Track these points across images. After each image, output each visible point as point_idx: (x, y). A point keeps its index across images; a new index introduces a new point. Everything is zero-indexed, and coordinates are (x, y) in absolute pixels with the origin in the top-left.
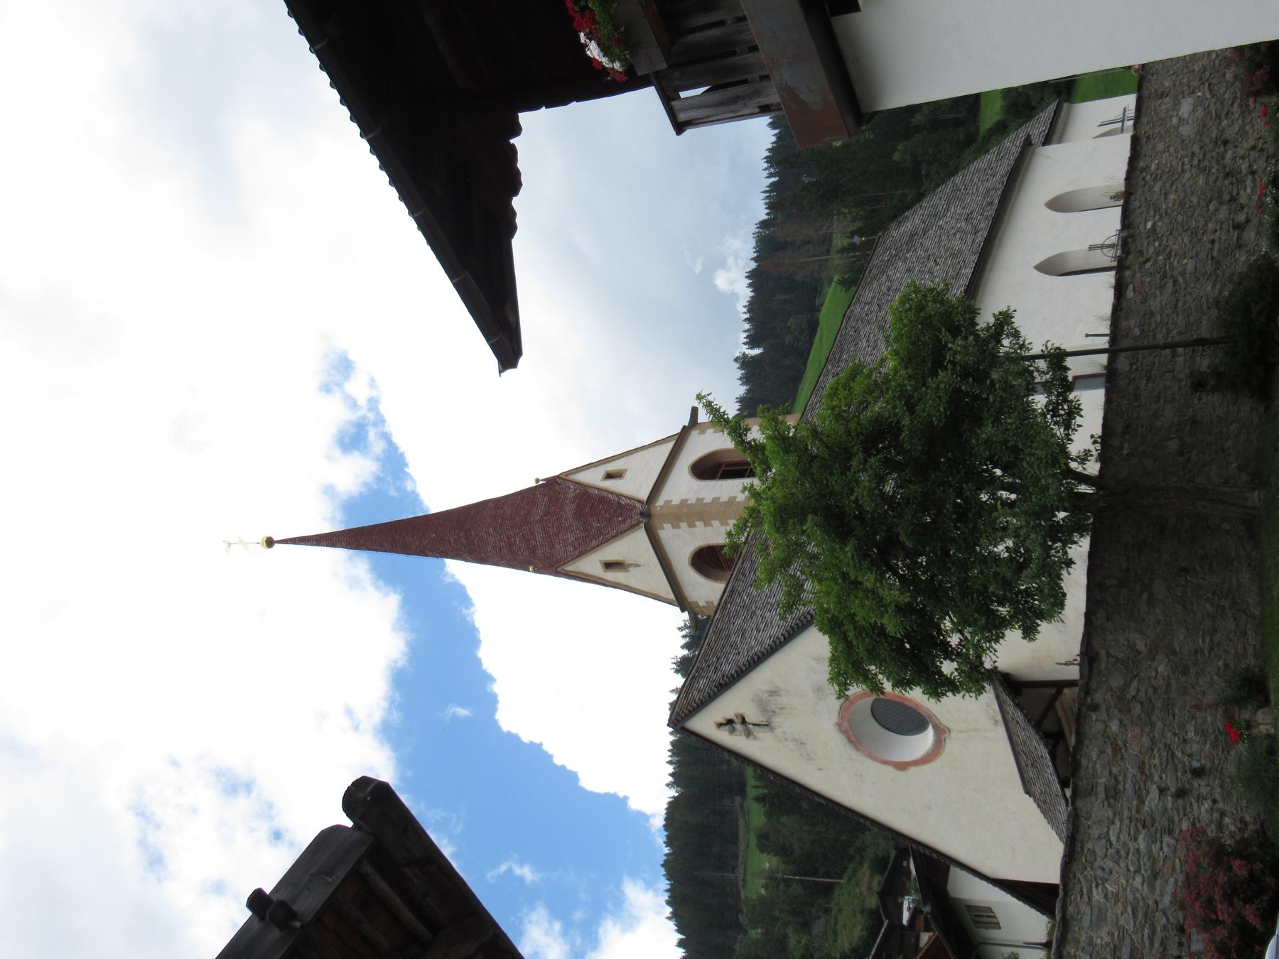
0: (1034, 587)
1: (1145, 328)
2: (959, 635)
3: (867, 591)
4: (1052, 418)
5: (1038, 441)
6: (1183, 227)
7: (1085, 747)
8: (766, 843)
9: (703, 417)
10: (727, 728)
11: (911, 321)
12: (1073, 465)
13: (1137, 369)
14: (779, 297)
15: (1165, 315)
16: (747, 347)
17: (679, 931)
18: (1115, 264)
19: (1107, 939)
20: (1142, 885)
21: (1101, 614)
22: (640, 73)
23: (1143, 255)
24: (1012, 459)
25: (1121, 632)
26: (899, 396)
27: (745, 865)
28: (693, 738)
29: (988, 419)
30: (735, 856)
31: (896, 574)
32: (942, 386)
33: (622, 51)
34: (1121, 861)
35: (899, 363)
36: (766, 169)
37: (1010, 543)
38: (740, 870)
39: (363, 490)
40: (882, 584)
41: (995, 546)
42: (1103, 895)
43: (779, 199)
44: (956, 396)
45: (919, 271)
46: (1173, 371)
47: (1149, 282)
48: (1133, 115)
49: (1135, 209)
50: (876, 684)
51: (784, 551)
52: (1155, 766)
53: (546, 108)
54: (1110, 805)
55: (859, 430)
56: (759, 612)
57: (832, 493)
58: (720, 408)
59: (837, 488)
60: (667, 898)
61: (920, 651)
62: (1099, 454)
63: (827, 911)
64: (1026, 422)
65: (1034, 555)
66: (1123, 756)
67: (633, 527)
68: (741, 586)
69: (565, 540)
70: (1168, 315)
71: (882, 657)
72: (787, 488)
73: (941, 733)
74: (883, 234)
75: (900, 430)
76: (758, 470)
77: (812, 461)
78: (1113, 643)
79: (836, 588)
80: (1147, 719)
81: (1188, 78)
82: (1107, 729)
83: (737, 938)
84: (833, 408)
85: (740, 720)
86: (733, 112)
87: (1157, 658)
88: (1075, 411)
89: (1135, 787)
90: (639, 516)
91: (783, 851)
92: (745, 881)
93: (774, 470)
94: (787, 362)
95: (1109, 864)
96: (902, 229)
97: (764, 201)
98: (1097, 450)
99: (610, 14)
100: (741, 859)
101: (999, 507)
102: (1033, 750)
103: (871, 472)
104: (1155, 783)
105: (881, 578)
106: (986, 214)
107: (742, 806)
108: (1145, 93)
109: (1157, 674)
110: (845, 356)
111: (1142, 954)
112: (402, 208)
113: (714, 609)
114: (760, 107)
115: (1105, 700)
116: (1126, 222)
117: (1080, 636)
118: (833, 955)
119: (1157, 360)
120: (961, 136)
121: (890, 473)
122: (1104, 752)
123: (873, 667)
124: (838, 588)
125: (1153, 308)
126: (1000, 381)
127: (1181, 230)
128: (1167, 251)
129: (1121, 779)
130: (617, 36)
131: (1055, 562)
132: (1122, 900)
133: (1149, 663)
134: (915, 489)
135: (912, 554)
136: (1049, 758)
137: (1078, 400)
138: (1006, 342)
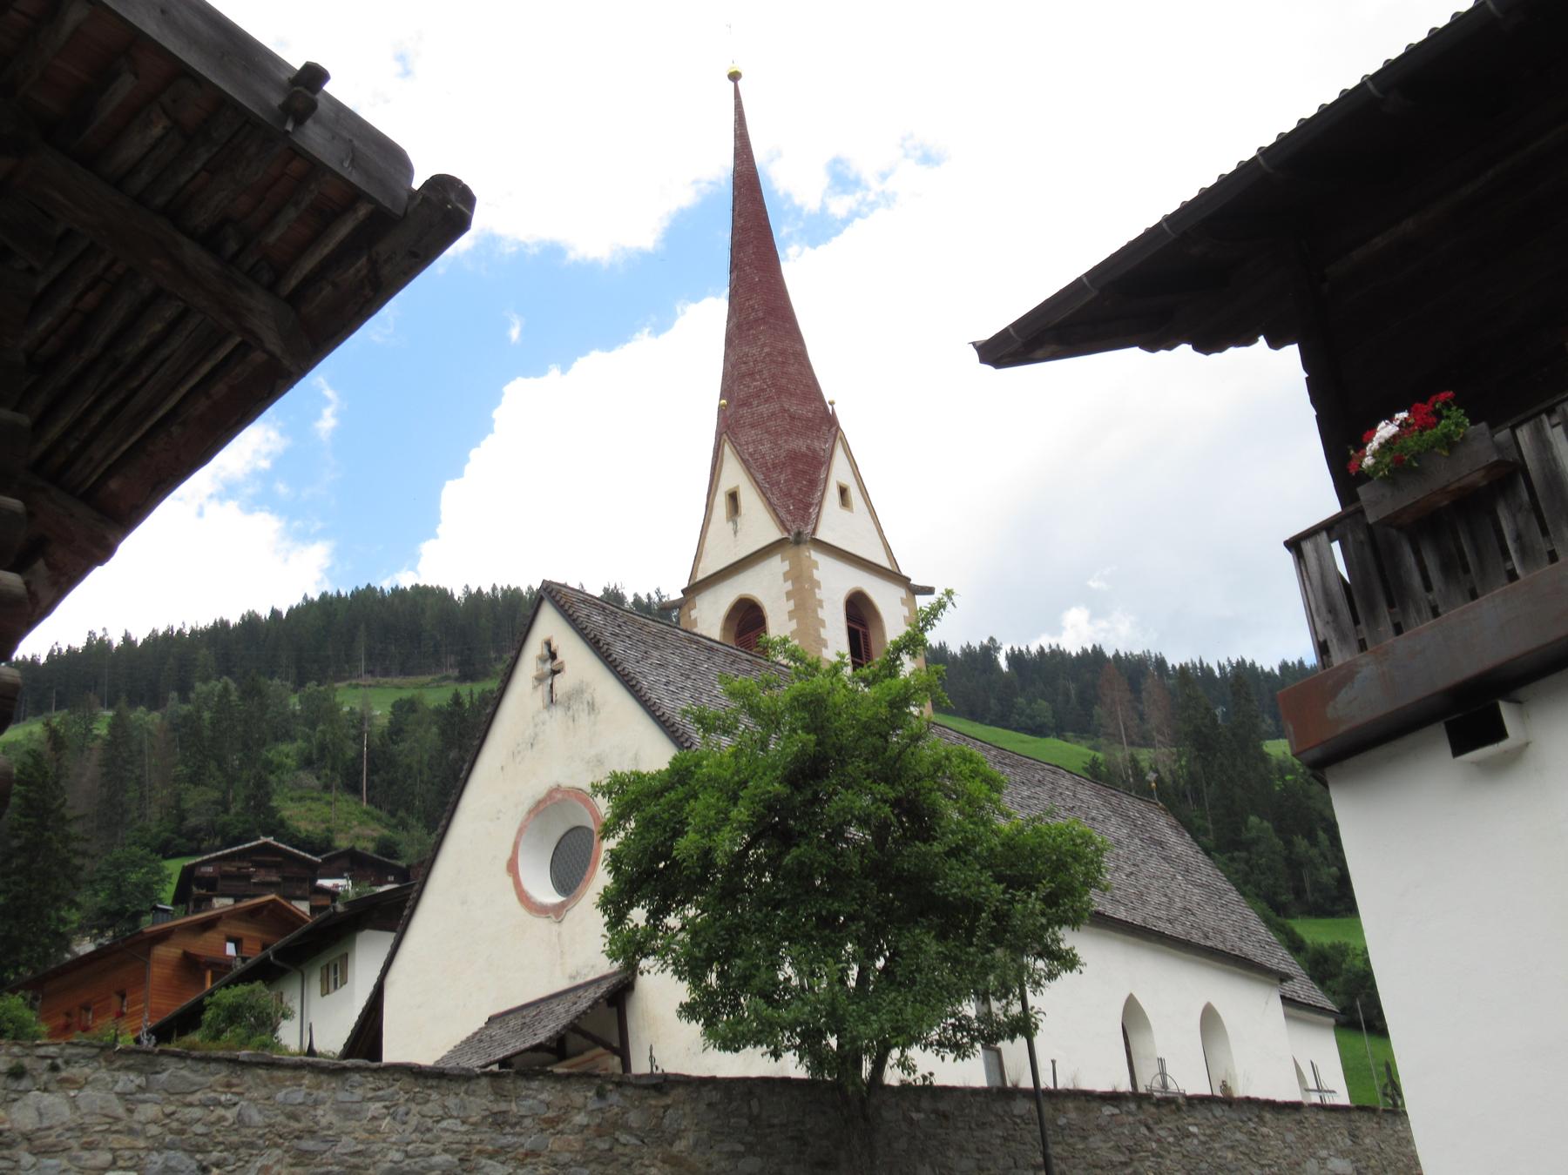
0: (744, 1013)
1: (1067, 1132)
2: (679, 926)
3: (727, 812)
4: (952, 1024)
5: (922, 1009)
6: (1192, 1170)
7: (552, 1085)
8: (404, 709)
9: (923, 602)
10: (546, 652)
11: (1060, 847)
12: (895, 1053)
13: (1015, 1123)
14: (1072, 687)
15: (1085, 1154)
16: (1009, 652)
17: (291, 611)
18: (1142, 1089)
19: (324, 1122)
20: (391, 1161)
21: (716, 1096)
22: (1361, 490)
23: (1156, 1123)
24: (898, 979)
25: (696, 1121)
26: (967, 838)
27: (375, 686)
28: (530, 613)
29: (946, 947)
30: (386, 673)
31: (749, 846)
32: (983, 889)
33: (1387, 466)
34: (418, 1135)
35: (1007, 836)
36: (1229, 661)
37: (795, 982)
38: (370, 680)
39: (781, 193)
40: (737, 830)
41: (790, 964)
42: (376, 1114)
43: (1193, 680)
44: (972, 907)
45: (1118, 855)
46: (1016, 1167)
47: (1123, 1133)
48: (1328, 1102)
49: (1211, 1111)
50: (612, 831)
51: (769, 708)
52: (536, 1169)
53: (1307, 379)
54: (485, 1118)
55: (922, 791)
56: (689, 683)
57: (843, 763)
58: (939, 619)
59: (850, 768)
60: (330, 593)
61: (656, 880)
62: (910, 1084)
63: (327, 788)
64: (945, 993)
65: (783, 1012)
66: (546, 1130)
67: (782, 524)
68: (719, 660)
69: (761, 442)
70: (1084, 1157)
71: (647, 835)
72: (847, 707)
73: (557, 912)
74: (1161, 808)
75: (925, 841)
76: (865, 671)
77: (881, 736)
78: (681, 1112)
79: (727, 775)
80: (592, 1158)
81: (1377, 1167)
82: (576, 1111)
83: (287, 680)
84: (947, 758)
85: (555, 668)
86: (1318, 609)
87: (666, 1166)
88: (960, 1051)
89: (509, 1147)
90: (796, 530)
91: (396, 731)
92: (357, 686)
93: (866, 690)
94: (993, 701)
95: (414, 1121)
96: (1168, 831)
97: (1189, 662)
98: (915, 1081)
99: (1433, 447)
100: (382, 680)
101: (841, 966)
102: (543, 1024)
103: (873, 808)
104: (515, 1170)
105: (742, 827)
106: (1194, 931)
107: (447, 678)
108: (1355, 1116)
109: (647, 1166)
110: (1008, 770)
111: (308, 1165)
112: (1172, 206)
113: (689, 629)
114: (1325, 642)
115: (611, 1105)
116: (1196, 1102)
117: (686, 1073)
118: (274, 797)
119: (1029, 1147)
120: (1284, 897)
121: (872, 834)
122: (548, 1108)
123: (633, 824)
124: (728, 777)
125: (1091, 1139)
126: (993, 959)
127: (1188, 1167)
128: (1162, 1153)
129: (518, 1129)
130: (1406, 458)
131: (777, 1037)
132: (372, 1137)
133: (660, 1156)
134: (855, 864)
135: (774, 863)
136: (534, 1043)
137: (974, 1054)
138: (1040, 964)
